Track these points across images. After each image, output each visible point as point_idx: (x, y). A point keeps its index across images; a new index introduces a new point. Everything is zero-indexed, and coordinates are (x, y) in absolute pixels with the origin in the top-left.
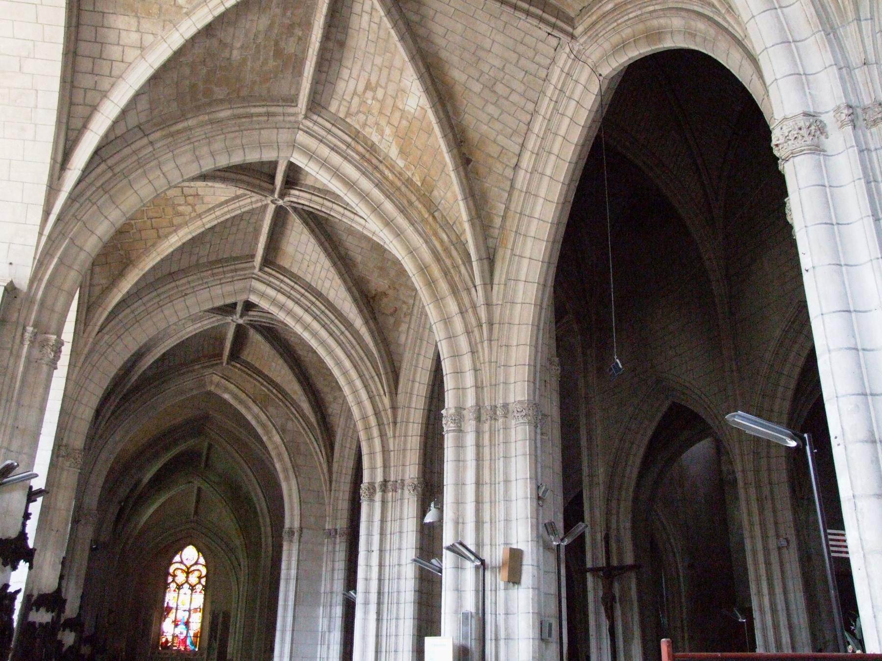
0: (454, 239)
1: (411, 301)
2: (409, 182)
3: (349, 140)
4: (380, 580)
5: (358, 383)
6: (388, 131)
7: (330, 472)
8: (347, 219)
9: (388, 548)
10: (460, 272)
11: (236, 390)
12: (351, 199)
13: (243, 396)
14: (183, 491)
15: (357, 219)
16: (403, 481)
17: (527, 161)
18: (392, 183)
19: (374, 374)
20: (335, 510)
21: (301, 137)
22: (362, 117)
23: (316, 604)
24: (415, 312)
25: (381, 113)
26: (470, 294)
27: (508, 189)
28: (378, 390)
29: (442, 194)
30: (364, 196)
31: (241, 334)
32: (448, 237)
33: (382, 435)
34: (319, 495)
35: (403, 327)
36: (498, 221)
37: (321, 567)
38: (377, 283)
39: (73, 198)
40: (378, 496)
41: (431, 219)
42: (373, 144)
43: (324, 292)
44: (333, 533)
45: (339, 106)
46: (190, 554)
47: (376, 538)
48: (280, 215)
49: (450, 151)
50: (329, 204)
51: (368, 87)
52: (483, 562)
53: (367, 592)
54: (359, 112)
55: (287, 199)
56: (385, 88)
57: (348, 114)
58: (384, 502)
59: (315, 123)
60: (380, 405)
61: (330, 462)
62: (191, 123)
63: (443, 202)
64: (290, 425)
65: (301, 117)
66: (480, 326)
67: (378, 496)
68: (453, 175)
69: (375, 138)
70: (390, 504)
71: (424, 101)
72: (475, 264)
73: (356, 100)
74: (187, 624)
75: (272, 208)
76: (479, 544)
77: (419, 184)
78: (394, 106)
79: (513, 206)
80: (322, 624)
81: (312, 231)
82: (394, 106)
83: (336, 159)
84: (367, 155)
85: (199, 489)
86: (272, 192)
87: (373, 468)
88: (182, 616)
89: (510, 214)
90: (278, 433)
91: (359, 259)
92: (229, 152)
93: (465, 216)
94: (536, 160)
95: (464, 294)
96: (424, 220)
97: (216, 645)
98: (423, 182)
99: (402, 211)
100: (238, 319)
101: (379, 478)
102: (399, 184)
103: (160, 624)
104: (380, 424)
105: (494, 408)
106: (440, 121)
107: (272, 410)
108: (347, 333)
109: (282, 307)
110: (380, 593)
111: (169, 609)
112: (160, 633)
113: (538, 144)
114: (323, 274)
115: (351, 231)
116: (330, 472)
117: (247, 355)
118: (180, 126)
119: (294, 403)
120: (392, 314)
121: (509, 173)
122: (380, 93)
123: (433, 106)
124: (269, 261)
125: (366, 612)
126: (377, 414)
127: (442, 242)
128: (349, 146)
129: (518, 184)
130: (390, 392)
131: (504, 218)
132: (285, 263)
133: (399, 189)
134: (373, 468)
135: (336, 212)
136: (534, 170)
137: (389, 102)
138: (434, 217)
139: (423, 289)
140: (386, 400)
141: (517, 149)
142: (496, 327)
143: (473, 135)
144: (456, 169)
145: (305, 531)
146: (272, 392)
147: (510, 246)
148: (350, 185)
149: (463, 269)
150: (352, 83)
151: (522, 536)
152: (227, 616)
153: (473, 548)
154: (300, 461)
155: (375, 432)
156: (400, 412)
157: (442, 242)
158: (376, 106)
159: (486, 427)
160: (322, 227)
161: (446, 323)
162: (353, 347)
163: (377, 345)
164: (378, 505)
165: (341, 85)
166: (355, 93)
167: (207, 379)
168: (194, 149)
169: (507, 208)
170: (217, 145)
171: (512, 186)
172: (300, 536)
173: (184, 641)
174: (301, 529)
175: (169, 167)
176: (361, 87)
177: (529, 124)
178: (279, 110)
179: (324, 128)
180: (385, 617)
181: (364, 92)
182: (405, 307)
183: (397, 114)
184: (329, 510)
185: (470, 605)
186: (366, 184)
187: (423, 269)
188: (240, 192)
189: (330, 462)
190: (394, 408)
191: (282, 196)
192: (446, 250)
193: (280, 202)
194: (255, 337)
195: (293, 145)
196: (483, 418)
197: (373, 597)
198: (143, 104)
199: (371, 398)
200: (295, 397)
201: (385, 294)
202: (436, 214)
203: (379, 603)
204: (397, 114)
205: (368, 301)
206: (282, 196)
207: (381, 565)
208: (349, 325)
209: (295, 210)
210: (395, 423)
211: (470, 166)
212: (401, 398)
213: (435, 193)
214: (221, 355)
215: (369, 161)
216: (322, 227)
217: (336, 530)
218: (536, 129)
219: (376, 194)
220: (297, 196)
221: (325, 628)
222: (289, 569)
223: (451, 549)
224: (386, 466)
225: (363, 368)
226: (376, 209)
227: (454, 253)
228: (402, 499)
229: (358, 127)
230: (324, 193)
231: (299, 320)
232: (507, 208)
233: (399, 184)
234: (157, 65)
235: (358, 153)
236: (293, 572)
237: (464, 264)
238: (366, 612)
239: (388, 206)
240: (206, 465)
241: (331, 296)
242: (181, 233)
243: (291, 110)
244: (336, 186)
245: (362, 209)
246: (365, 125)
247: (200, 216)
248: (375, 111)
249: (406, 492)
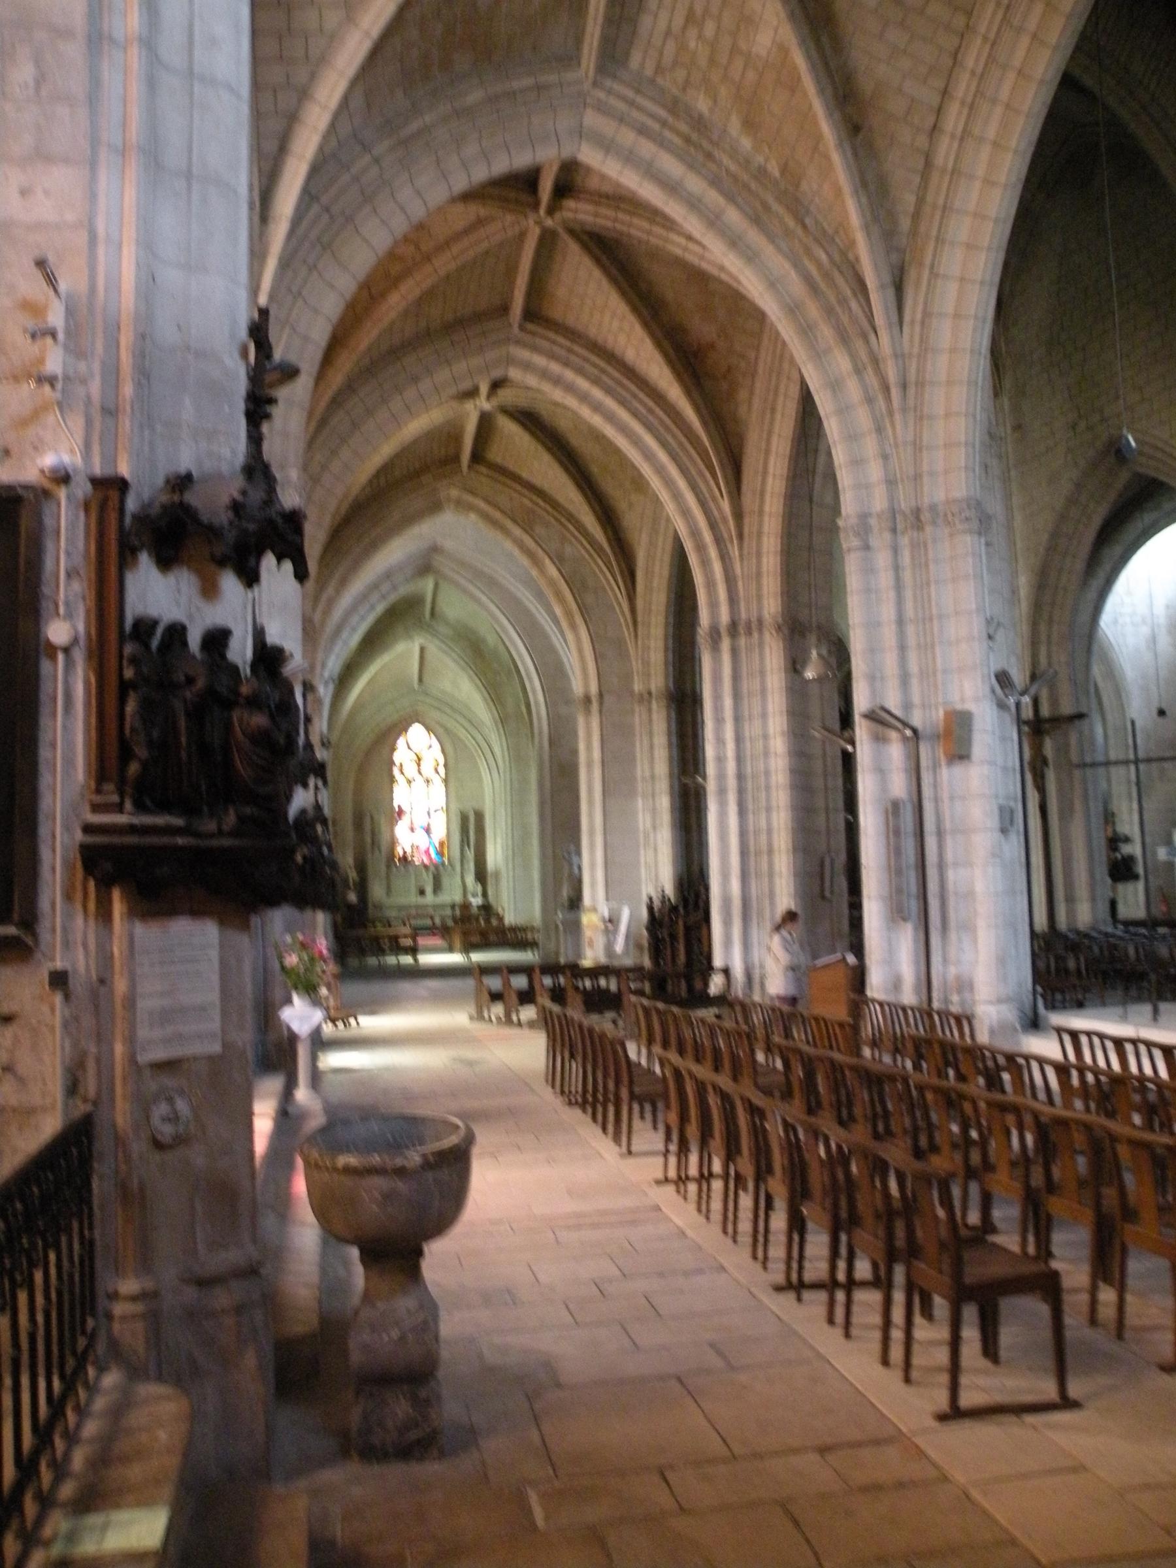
0: (837, 257)
1: (752, 355)
2: (761, 174)
3: (663, 113)
4: (739, 759)
5: (682, 484)
6: (723, 92)
7: (633, 610)
8: (656, 236)
9: (746, 713)
10: (850, 309)
11: (482, 505)
12: (674, 209)
13: (498, 515)
14: (404, 653)
15: (691, 246)
16: (760, 621)
17: (953, 119)
18: (735, 179)
19: (702, 467)
20: (646, 663)
21: (591, 119)
22: (680, 74)
23: (632, 794)
24: (760, 371)
25: (712, 61)
26: (867, 342)
27: (920, 167)
28: (710, 490)
29: (815, 186)
30: (694, 204)
31: (485, 424)
32: (827, 253)
33: (724, 557)
34: (620, 644)
35: (743, 395)
36: (905, 224)
37: (634, 745)
38: (702, 330)
39: (285, 264)
40: (726, 644)
41: (799, 231)
42: (701, 116)
43: (618, 352)
44: (646, 696)
45: (644, 58)
46: (417, 732)
47: (728, 702)
48: (548, 241)
49: (830, 115)
50: (627, 218)
51: (690, 18)
52: (915, 731)
53: (721, 776)
54: (675, 63)
55: (558, 216)
56: (719, 19)
57: (659, 69)
58: (734, 652)
59: (610, 92)
60: (716, 513)
61: (631, 598)
62: (428, 118)
63: (817, 200)
64: (568, 550)
65: (587, 86)
66: (886, 389)
67: (726, 644)
68: (836, 158)
69: (702, 105)
70: (743, 655)
71: (788, 35)
72: (874, 297)
73: (670, 47)
74: (428, 830)
75: (534, 233)
76: (907, 706)
77: (776, 173)
78: (734, 50)
79: (929, 198)
80: (643, 820)
81: (598, 261)
82: (734, 50)
83: (647, 149)
84: (694, 136)
85: (422, 650)
86: (536, 206)
87: (713, 605)
88: (420, 821)
89: (927, 209)
90: (554, 563)
91: (670, 296)
92: (486, 156)
93: (855, 219)
94: (969, 115)
95: (859, 344)
96: (788, 233)
97: (470, 855)
98: (784, 169)
99: (756, 221)
100: (484, 403)
101: (724, 617)
102: (745, 177)
103: (392, 831)
104: (718, 540)
105: (917, 512)
106: (813, 68)
107: (539, 530)
108: (658, 411)
109: (557, 381)
110: (740, 777)
111: (401, 812)
112: (393, 842)
113: (973, 88)
114: (616, 324)
115: (655, 254)
116: (633, 610)
117: (495, 454)
118: (414, 126)
119: (571, 518)
120: (725, 377)
121: (922, 141)
122: (710, 29)
123: (802, 42)
124: (532, 314)
125: (723, 804)
126: (713, 526)
127: (819, 265)
128: (664, 123)
129: (939, 160)
130: (729, 493)
131: (916, 216)
132: (556, 313)
133: (746, 186)
134: (713, 605)
135: (637, 229)
136: (966, 134)
137: (726, 42)
138: (804, 226)
139: (796, 341)
140: (726, 505)
141: (935, 100)
142: (912, 391)
143: (866, 86)
144: (840, 145)
145: (607, 698)
146: (537, 504)
147: (928, 261)
148: (672, 188)
149: (854, 305)
150: (663, 16)
151: (971, 692)
152: (479, 817)
153: (897, 712)
154: (590, 599)
155: (713, 553)
156: (746, 521)
157: (819, 265)
158: (703, 53)
159: (904, 541)
160: (616, 258)
161: (834, 391)
162: (667, 429)
163: (705, 424)
164: (726, 657)
165: (646, 21)
166: (668, 33)
167: (443, 495)
168: (438, 162)
169: (920, 201)
170: (471, 149)
171: (928, 164)
172: (601, 703)
173: (427, 852)
174: (601, 695)
175: (405, 194)
176: (679, 20)
177: (956, 54)
178: (553, 78)
179: (624, 99)
180: (750, 807)
181: (685, 28)
182: (743, 364)
183: (739, 63)
184: (636, 665)
185: (899, 786)
186: (695, 184)
187: (793, 310)
188: (483, 212)
189: (631, 598)
190: (738, 515)
191: (551, 211)
192: (826, 276)
193: (549, 222)
194: (508, 427)
195: (580, 133)
196: (899, 527)
197: (732, 783)
198: (357, 102)
199: (702, 503)
200: (571, 508)
201: (712, 346)
202: (808, 221)
203: (741, 791)
204: (739, 63)
205: (690, 360)
206: (551, 211)
207: (739, 740)
208: (658, 397)
209: (571, 232)
210: (740, 536)
211: (860, 137)
212: (748, 500)
213: (804, 186)
214: (456, 458)
215: (698, 147)
216: (616, 258)
217: (650, 693)
218: (970, 62)
219: (713, 197)
220: (578, 211)
221: (648, 824)
222: (589, 748)
223: (871, 716)
224: (733, 600)
225: (685, 459)
226: (713, 221)
227: (840, 281)
228: (761, 645)
229: (675, 91)
230: (622, 200)
231: (584, 398)
232: (920, 201)
233: (745, 177)
234: (376, 32)
235: (678, 133)
236: (597, 754)
237: (855, 295)
238: (723, 804)
239: (733, 216)
240: (433, 614)
241: (630, 356)
242: (404, 288)
243: (570, 76)
244: (649, 192)
245: (693, 225)
246: (686, 85)
247: (428, 258)
248: (703, 62)
249: (767, 637)
